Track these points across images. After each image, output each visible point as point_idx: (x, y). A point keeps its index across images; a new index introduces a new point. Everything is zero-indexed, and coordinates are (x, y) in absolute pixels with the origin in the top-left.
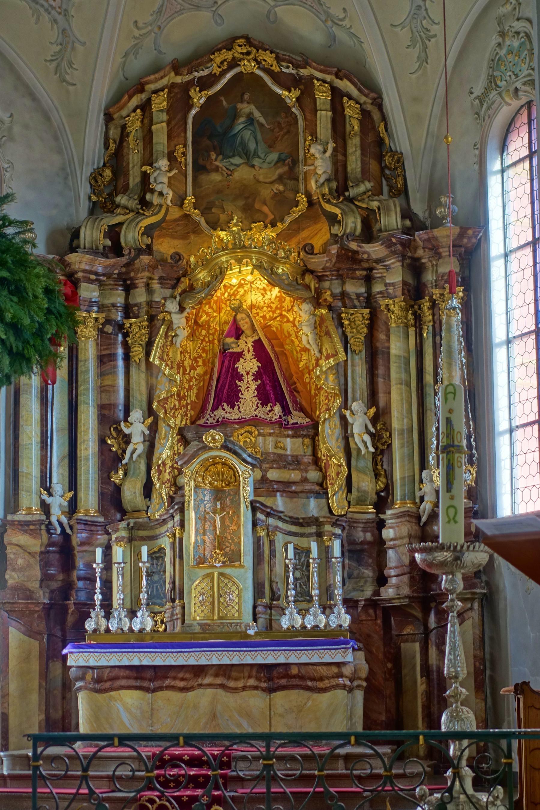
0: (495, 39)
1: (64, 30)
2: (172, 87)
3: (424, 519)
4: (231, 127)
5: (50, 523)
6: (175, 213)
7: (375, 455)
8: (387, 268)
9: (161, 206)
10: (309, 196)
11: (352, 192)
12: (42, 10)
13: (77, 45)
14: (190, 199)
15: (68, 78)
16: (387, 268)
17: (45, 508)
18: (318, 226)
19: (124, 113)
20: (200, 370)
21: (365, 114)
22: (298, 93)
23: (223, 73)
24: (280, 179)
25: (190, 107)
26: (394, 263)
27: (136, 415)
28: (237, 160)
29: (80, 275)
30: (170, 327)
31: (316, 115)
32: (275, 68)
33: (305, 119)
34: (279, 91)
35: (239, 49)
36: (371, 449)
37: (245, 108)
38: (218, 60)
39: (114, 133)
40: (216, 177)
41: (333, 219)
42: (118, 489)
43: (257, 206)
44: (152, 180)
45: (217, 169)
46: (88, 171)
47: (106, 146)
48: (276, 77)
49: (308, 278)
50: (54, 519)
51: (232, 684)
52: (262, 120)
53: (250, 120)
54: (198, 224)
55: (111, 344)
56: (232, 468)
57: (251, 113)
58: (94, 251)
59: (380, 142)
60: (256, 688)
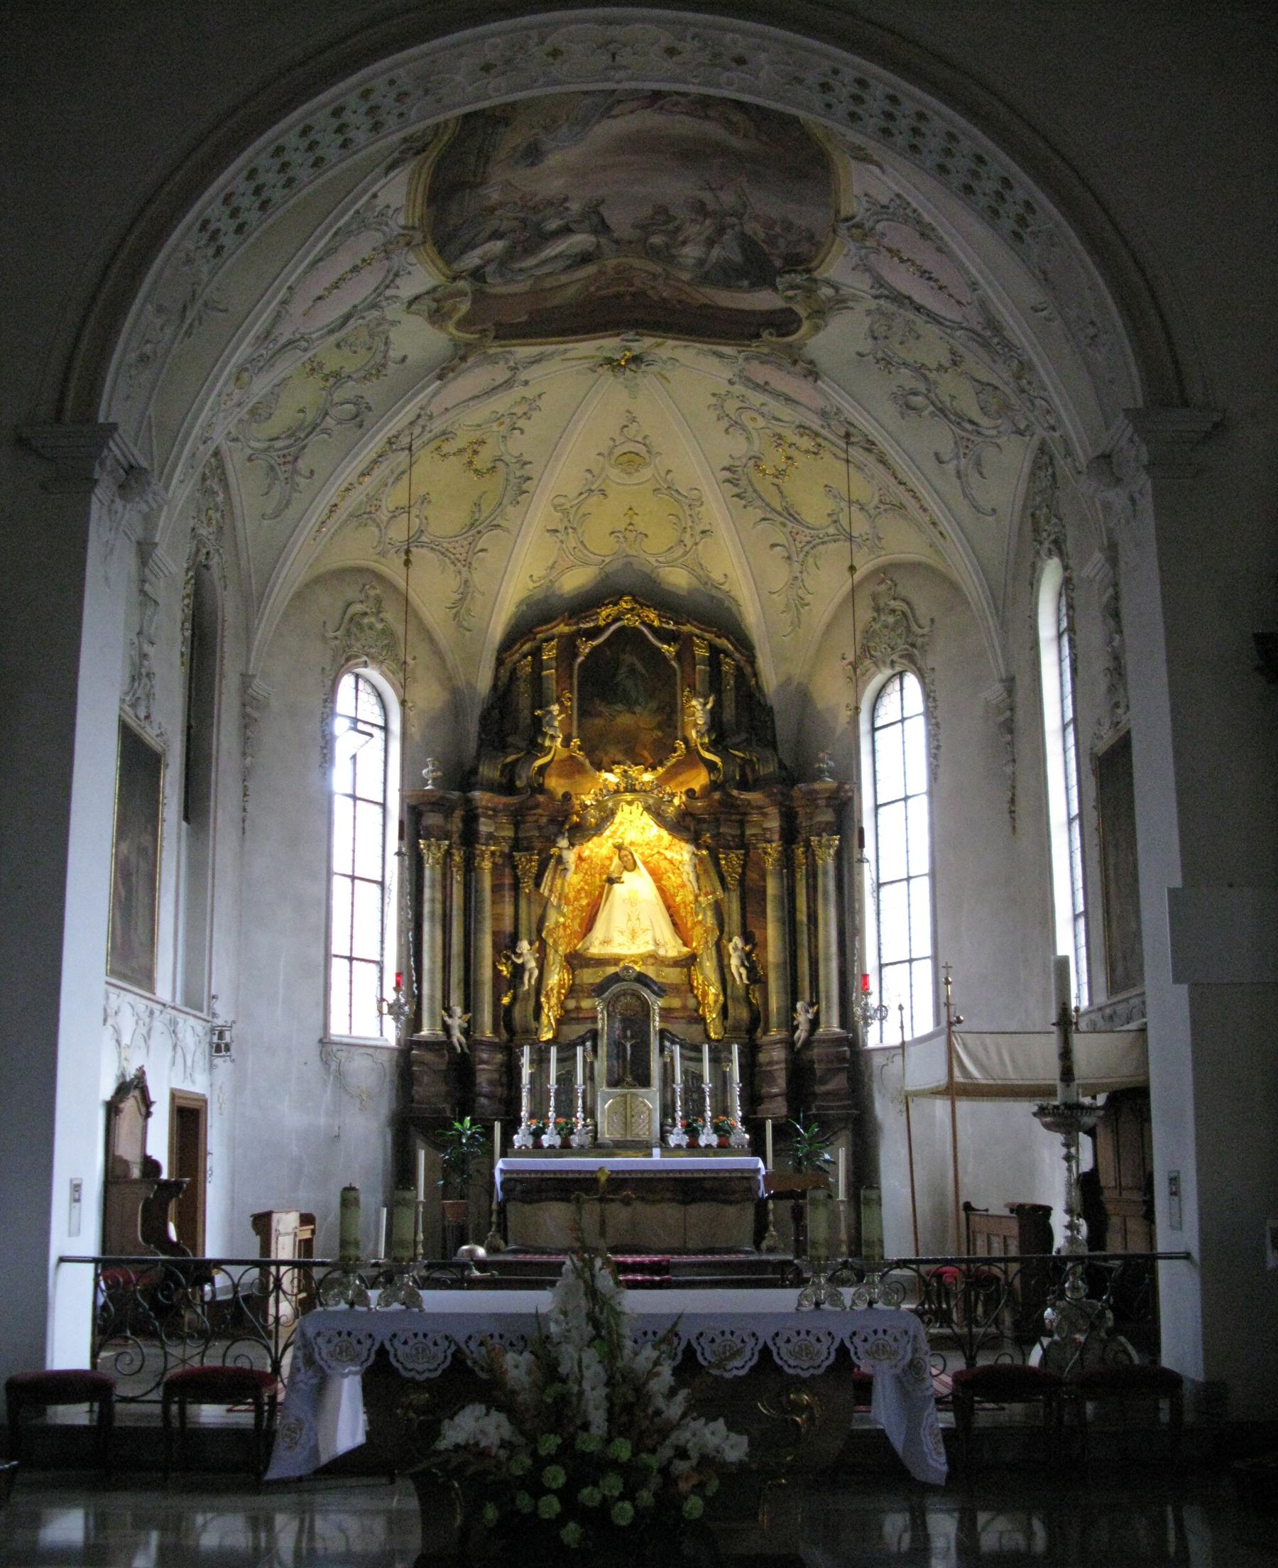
0: (870, 614)
1: (466, 581)
2: (561, 636)
3: (799, 1045)
4: (614, 675)
5: (451, 1043)
6: (563, 753)
7: (747, 987)
8: (765, 815)
9: (550, 748)
10: (686, 741)
11: (729, 741)
12: (448, 561)
13: (477, 595)
14: (576, 742)
15: (465, 624)
16: (765, 815)
17: (447, 1028)
18: (694, 772)
19: (517, 656)
20: (584, 902)
21: (739, 668)
22: (677, 647)
23: (608, 625)
24: (659, 726)
25: (576, 655)
26: (773, 811)
27: (524, 946)
28: (619, 707)
29: (480, 810)
30: (560, 860)
31: (694, 668)
32: (656, 623)
33: (683, 672)
34: (659, 645)
35: (624, 605)
36: (746, 982)
37: (629, 659)
38: (604, 614)
39: (504, 672)
40: (599, 722)
41: (711, 766)
42: (509, 1009)
43: (637, 750)
44: (544, 722)
45: (600, 714)
46: (477, 712)
47: (495, 687)
48: (656, 632)
49: (688, 819)
50: (455, 1040)
51: (650, 1197)
52: (644, 672)
53: (632, 671)
54: (582, 765)
55: (502, 875)
56: (639, 997)
57: (633, 664)
58: (491, 787)
59: (751, 696)
60: (673, 1200)
